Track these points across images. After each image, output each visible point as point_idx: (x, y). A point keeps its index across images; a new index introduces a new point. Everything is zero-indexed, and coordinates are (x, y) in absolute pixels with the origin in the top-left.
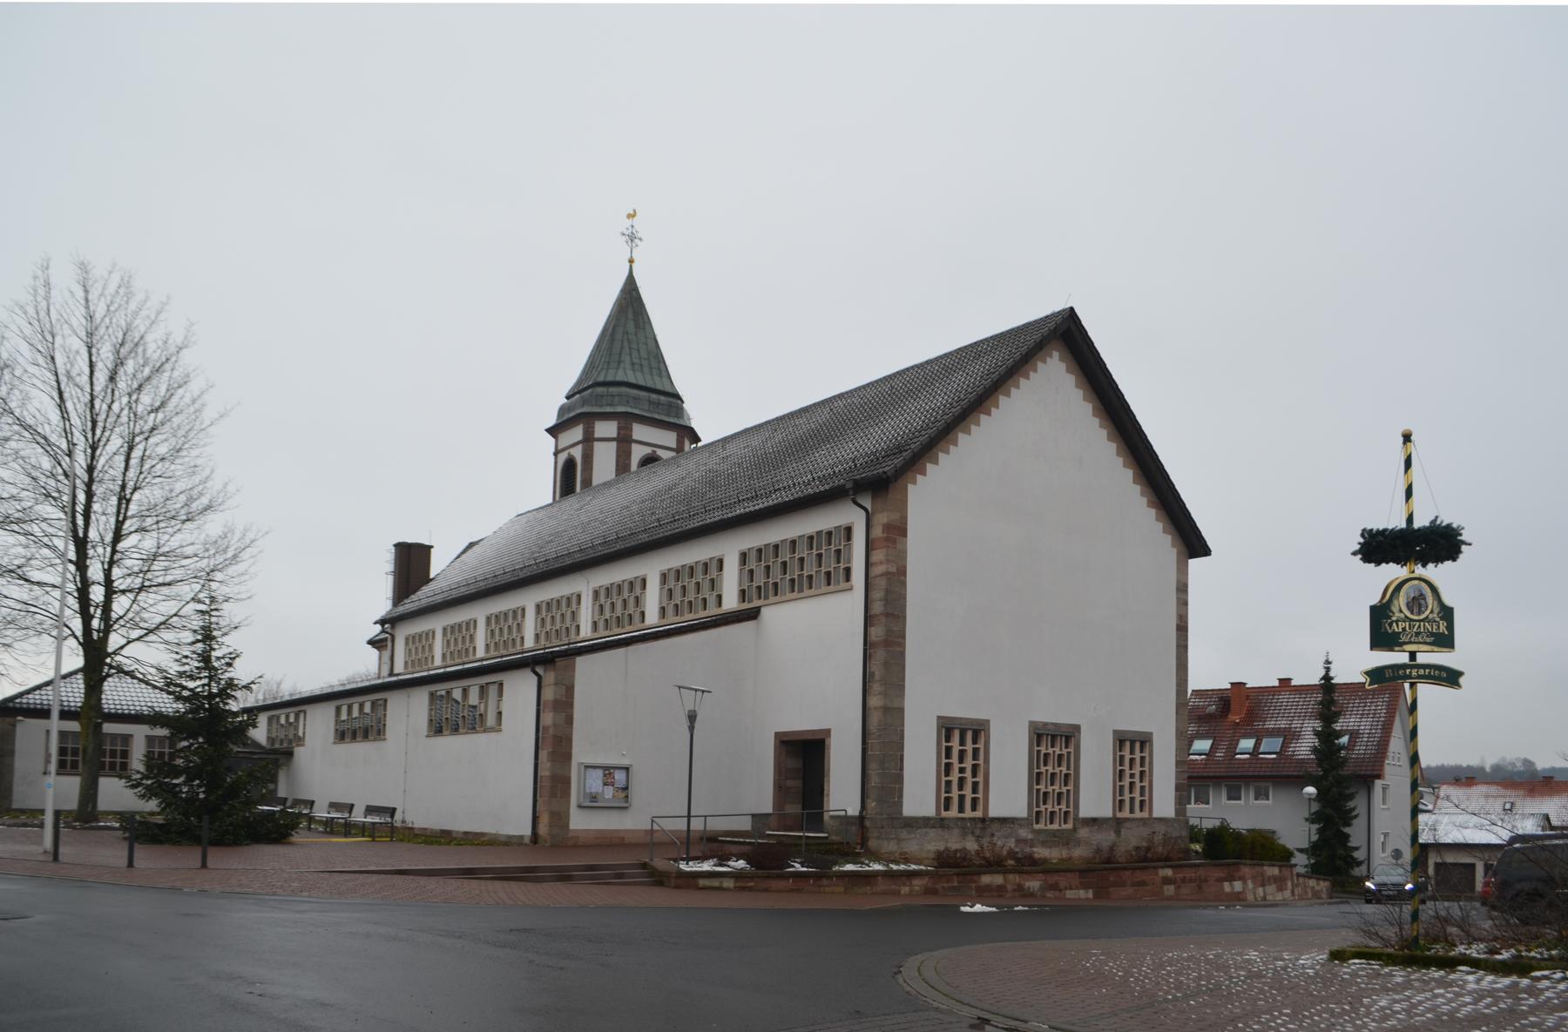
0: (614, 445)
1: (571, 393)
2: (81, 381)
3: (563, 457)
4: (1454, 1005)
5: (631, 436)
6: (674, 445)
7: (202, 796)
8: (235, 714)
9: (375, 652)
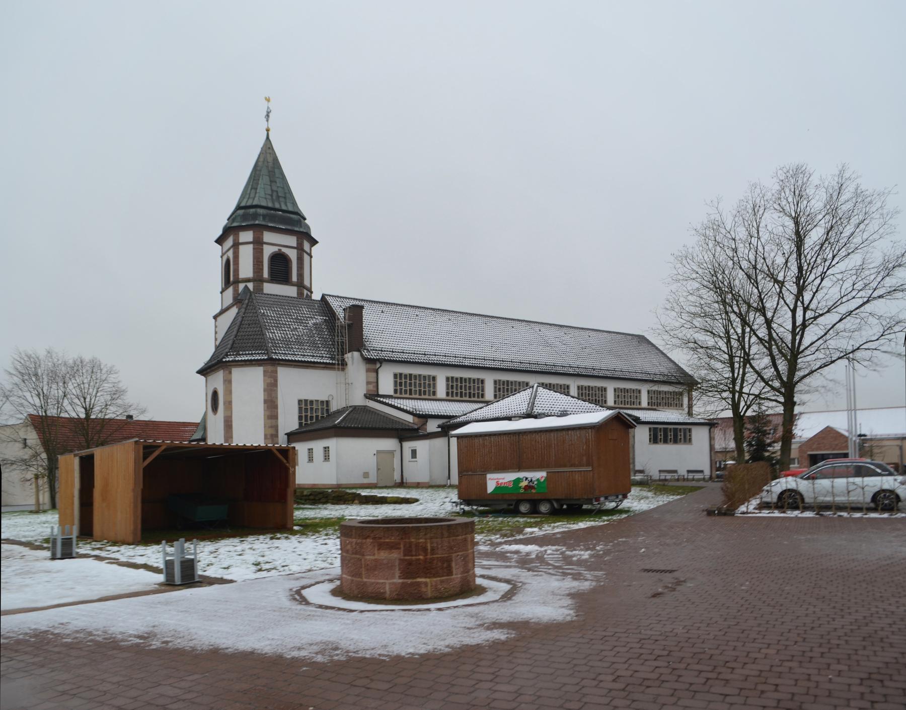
0: (251, 246)
2: (892, 348)
3: (225, 258)
4: (616, 542)
5: (262, 239)
6: (295, 245)
7: (864, 545)
9: (203, 378)
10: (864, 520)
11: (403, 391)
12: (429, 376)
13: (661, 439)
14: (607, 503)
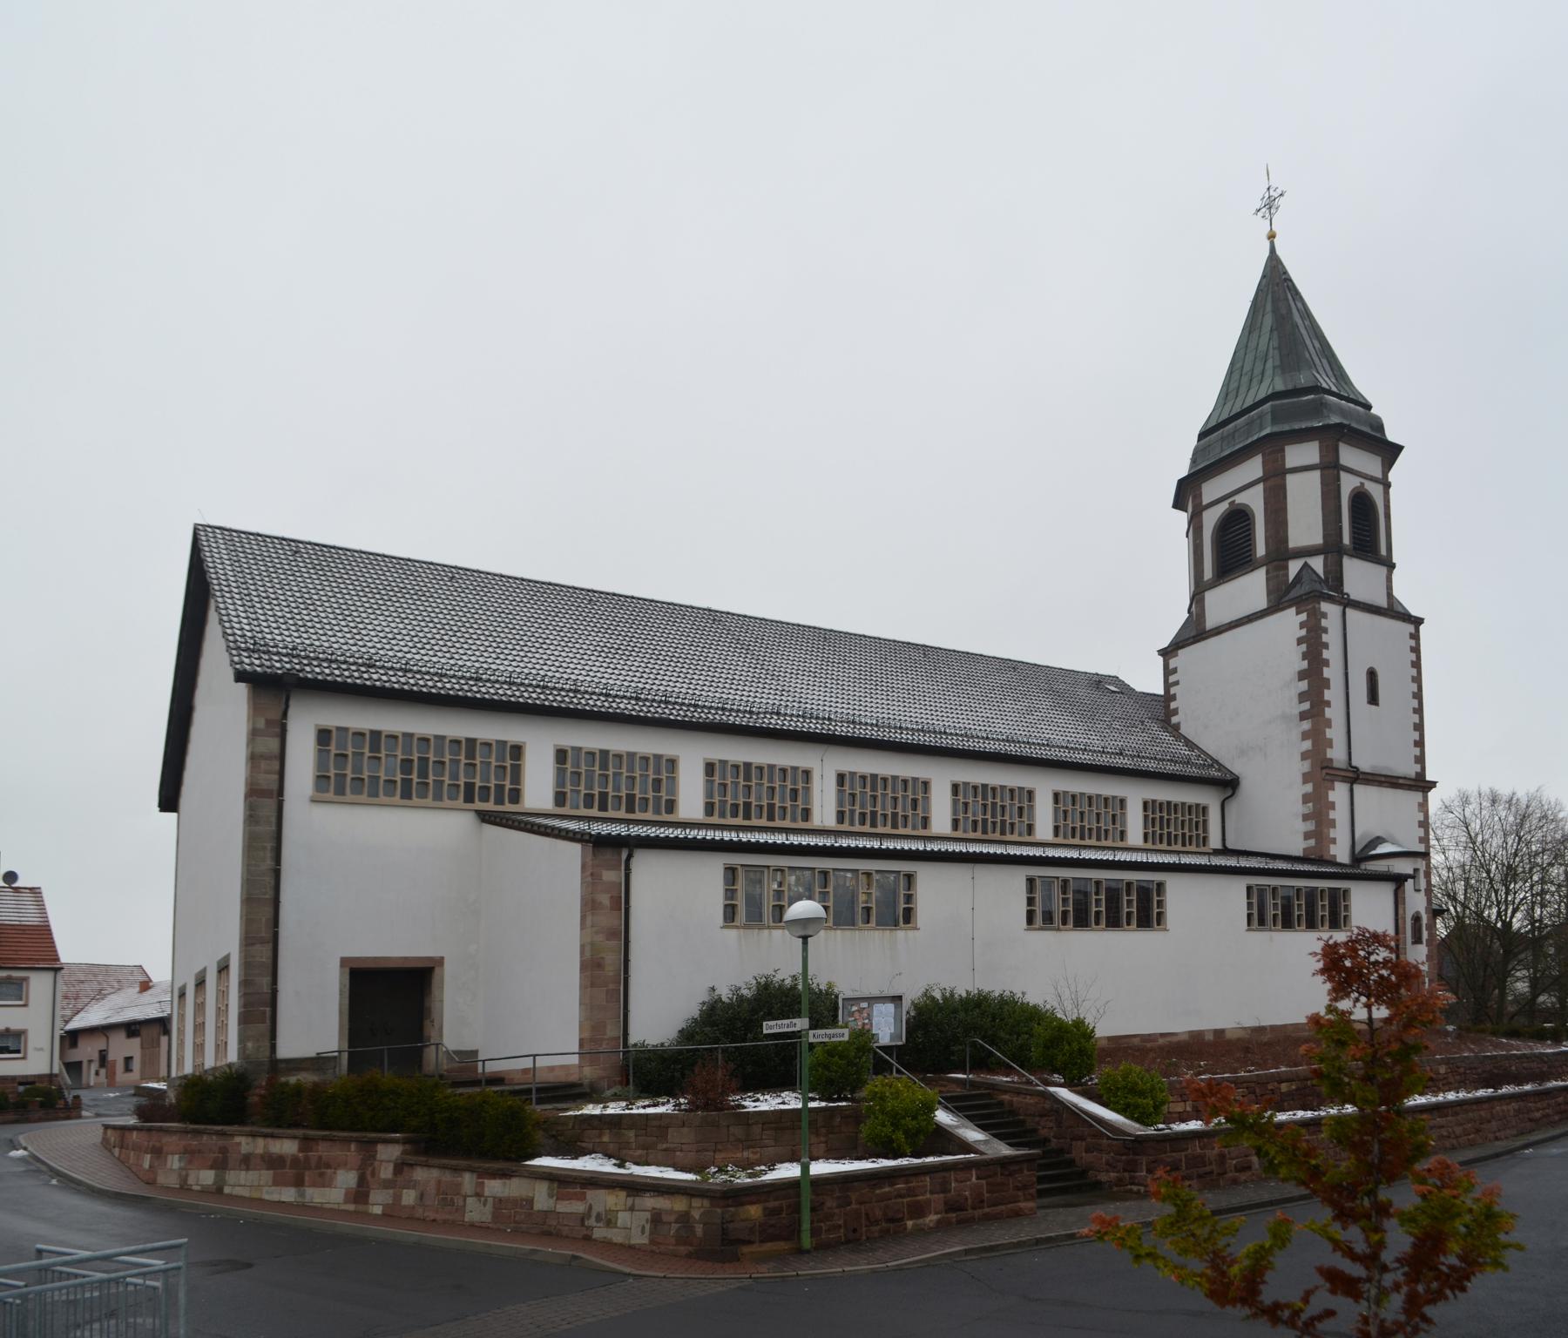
0: (1316, 475)
1: (1213, 423)
8: (1555, 996)
10: (908, 1151)
11: (799, 811)
12: (658, 757)
13: (1098, 914)
14: (527, 1108)
